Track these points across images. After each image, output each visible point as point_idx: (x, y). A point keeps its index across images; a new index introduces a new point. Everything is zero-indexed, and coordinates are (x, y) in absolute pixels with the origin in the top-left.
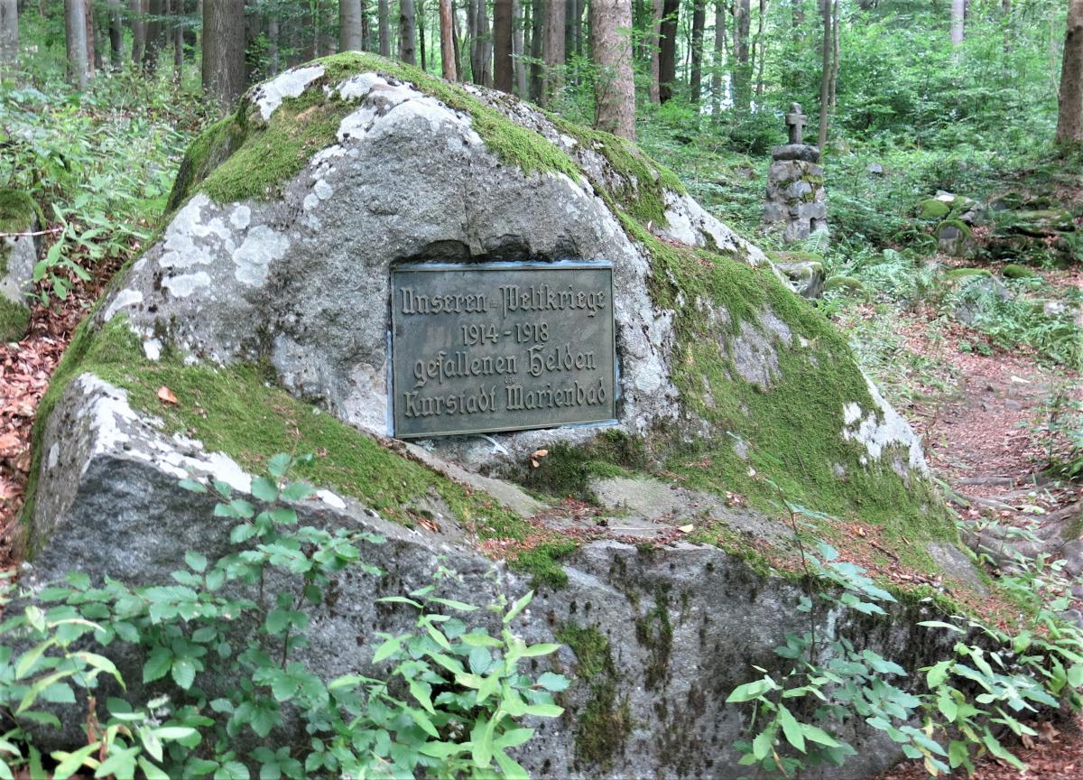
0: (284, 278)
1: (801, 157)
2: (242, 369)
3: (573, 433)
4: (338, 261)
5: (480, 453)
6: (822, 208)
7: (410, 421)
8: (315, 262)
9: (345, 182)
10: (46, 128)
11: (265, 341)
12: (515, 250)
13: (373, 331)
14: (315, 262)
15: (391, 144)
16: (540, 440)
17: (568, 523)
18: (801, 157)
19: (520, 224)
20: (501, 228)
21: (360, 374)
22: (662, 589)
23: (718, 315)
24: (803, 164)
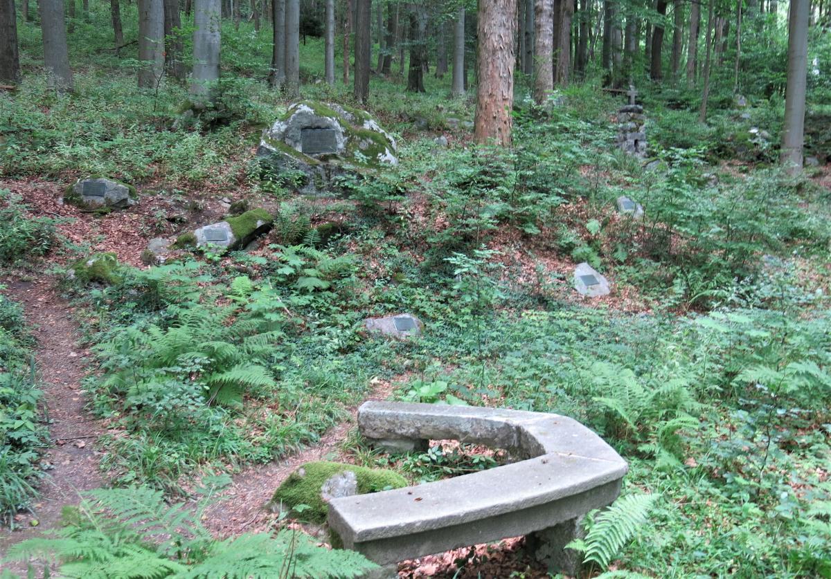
0: (287, 131)
1: (631, 111)
2: (281, 141)
3: (327, 153)
4: (294, 129)
5: (314, 155)
6: (642, 135)
7: (304, 150)
8: (291, 128)
9: (294, 118)
10: (668, 139)
11: (284, 138)
12: (319, 127)
13: (299, 138)
14: (291, 128)
15: (300, 114)
16: (322, 154)
17: (646, 273)
18: (631, 111)
19: (320, 124)
20: (316, 125)
21: (298, 144)
22: (330, 170)
23: (358, 138)
24: (632, 114)
